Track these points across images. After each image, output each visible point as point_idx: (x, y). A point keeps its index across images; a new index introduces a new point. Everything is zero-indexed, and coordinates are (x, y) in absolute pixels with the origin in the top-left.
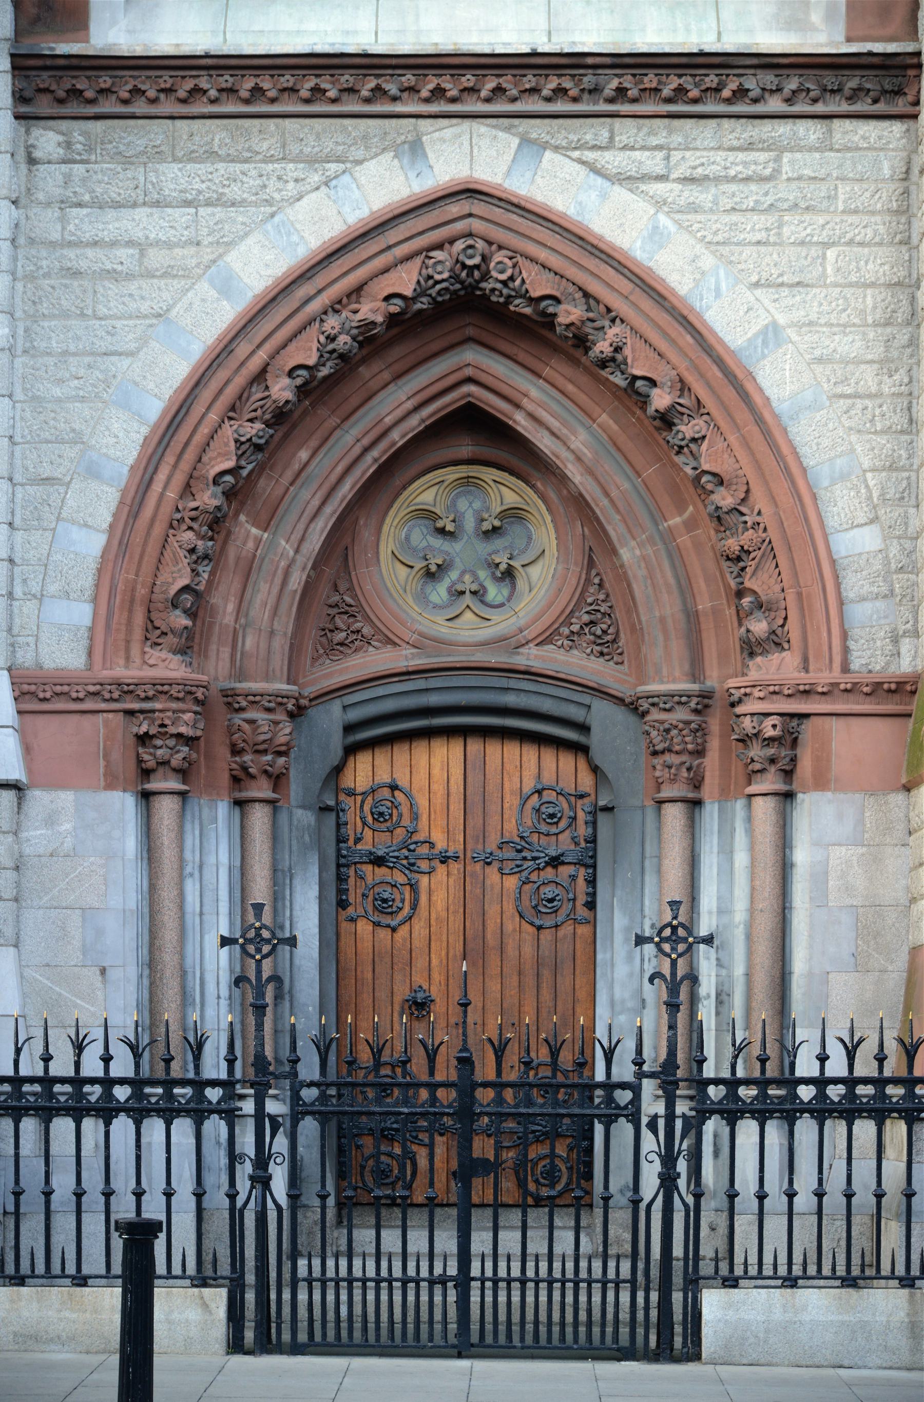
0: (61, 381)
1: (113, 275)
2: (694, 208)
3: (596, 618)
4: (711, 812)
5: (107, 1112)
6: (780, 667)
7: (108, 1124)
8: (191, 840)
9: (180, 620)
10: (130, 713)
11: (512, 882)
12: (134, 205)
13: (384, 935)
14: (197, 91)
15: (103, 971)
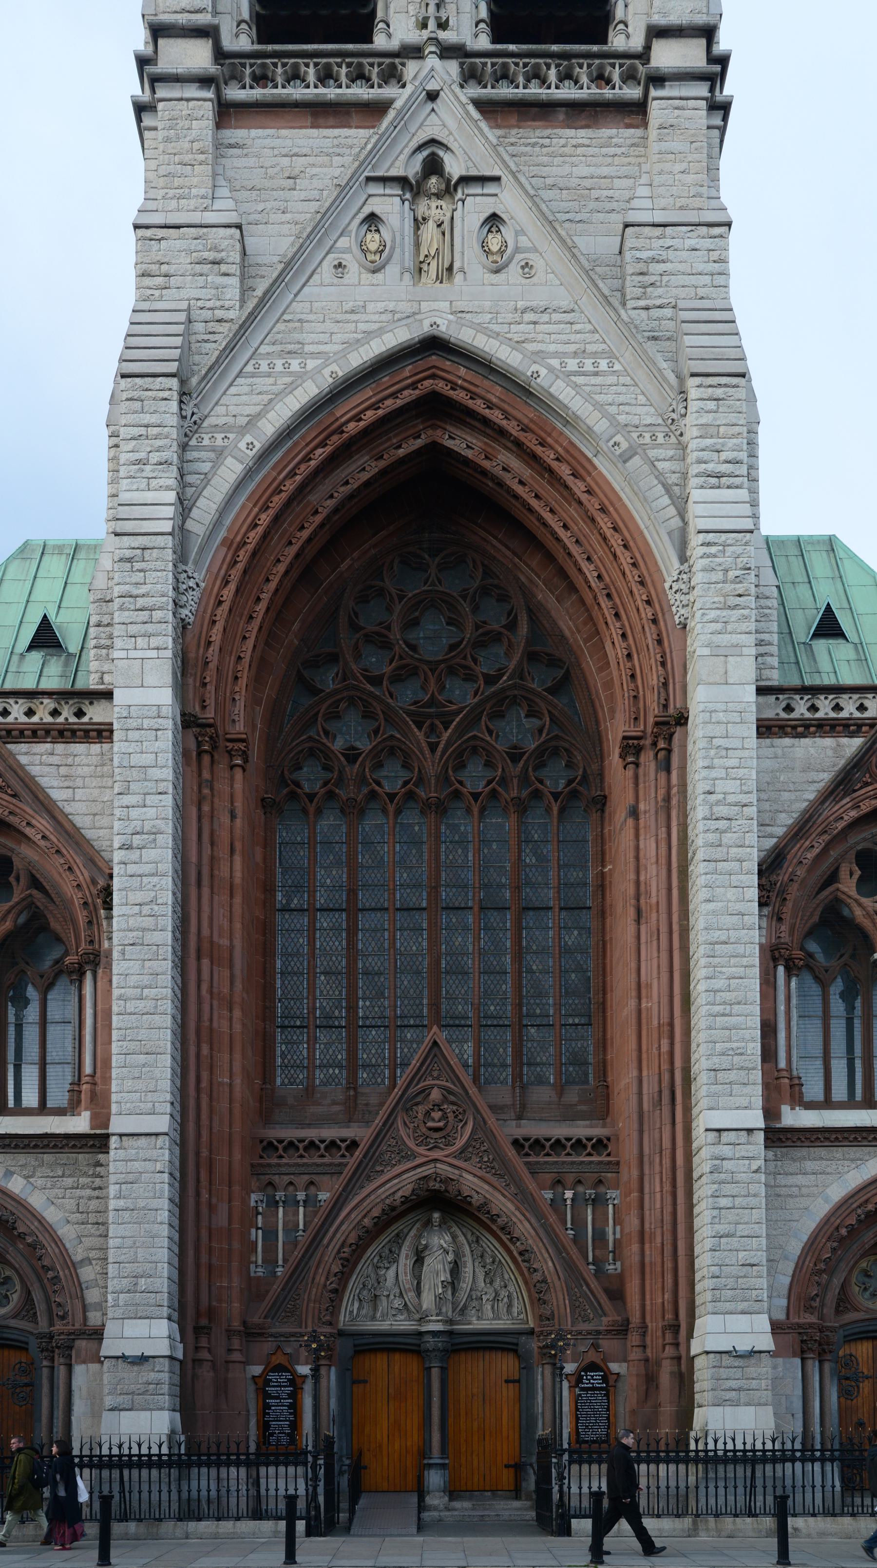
1: (791, 1196)
5: (793, 1460)
13: (849, 1402)
14: (818, 1138)
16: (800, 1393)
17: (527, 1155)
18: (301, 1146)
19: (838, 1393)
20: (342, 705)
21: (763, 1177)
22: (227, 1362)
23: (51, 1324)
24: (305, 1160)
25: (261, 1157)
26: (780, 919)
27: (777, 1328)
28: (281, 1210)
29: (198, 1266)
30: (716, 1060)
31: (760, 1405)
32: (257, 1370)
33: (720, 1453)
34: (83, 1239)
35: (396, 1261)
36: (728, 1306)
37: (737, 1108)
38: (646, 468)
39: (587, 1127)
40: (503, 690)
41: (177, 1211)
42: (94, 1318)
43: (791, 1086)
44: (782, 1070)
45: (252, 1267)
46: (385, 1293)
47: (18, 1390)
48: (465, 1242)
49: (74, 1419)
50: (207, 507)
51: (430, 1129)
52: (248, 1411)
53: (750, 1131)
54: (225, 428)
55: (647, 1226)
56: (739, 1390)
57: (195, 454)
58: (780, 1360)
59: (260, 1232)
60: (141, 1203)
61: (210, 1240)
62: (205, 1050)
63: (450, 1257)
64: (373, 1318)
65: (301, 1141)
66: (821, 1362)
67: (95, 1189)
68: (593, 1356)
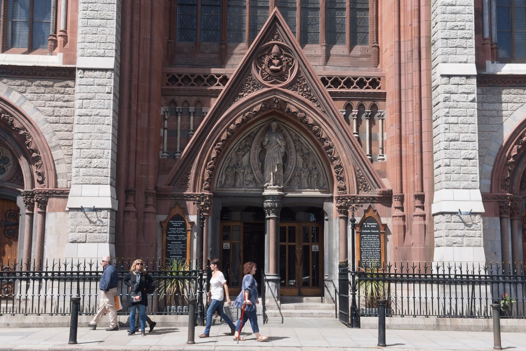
0: (483, 137)
1: (493, 117)
10: (499, 202)
12: (496, 103)
15: (495, 253)
17: (330, 87)
18: (206, 79)
19: (523, 239)
22: (145, 213)
23: (33, 186)
25: (168, 85)
27: (486, 199)
28: (179, 118)
29: (129, 152)
31: (476, 246)
32: (163, 217)
33: (452, 277)
34: (57, 133)
35: (249, 150)
36: (456, 184)
37: (460, 62)
39: (366, 71)
41: (117, 117)
42: (62, 184)
43: (492, 49)
44: (487, 39)
45: (161, 152)
47: (8, 228)
48: (291, 140)
49: (45, 247)
51: (272, 71)
52: (157, 244)
53: (468, 77)
55: (403, 133)
58: (487, 218)
59: (166, 131)
62: (136, 18)
63: (282, 150)
64: (234, 186)
65: (193, 76)
66: (512, 220)
67: (65, 101)
68: (370, 214)
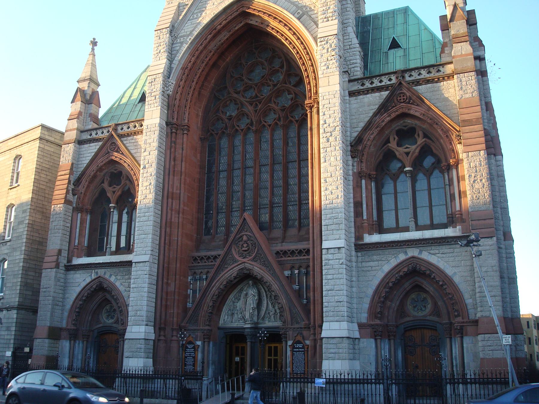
2: (443, 257)
3: (436, 311)
4: (453, 339)
6: (460, 319)
7: (75, 341)
8: (382, 345)
9: (379, 316)
11: (428, 349)
16: (374, 353)
20: (228, 103)
21: (344, 266)
24: (206, 264)
26: (362, 162)
27: (361, 326)
30: (327, 221)
36: (331, 319)
38: (308, 18)
40: (278, 88)
45: (188, 304)
46: (236, 312)
50: (176, 62)
51: (243, 251)
54: (182, 37)
56: (335, 353)
57: (175, 45)
60: (140, 285)
61: (167, 296)
63: (256, 298)
64: (232, 322)
68: (299, 338)
